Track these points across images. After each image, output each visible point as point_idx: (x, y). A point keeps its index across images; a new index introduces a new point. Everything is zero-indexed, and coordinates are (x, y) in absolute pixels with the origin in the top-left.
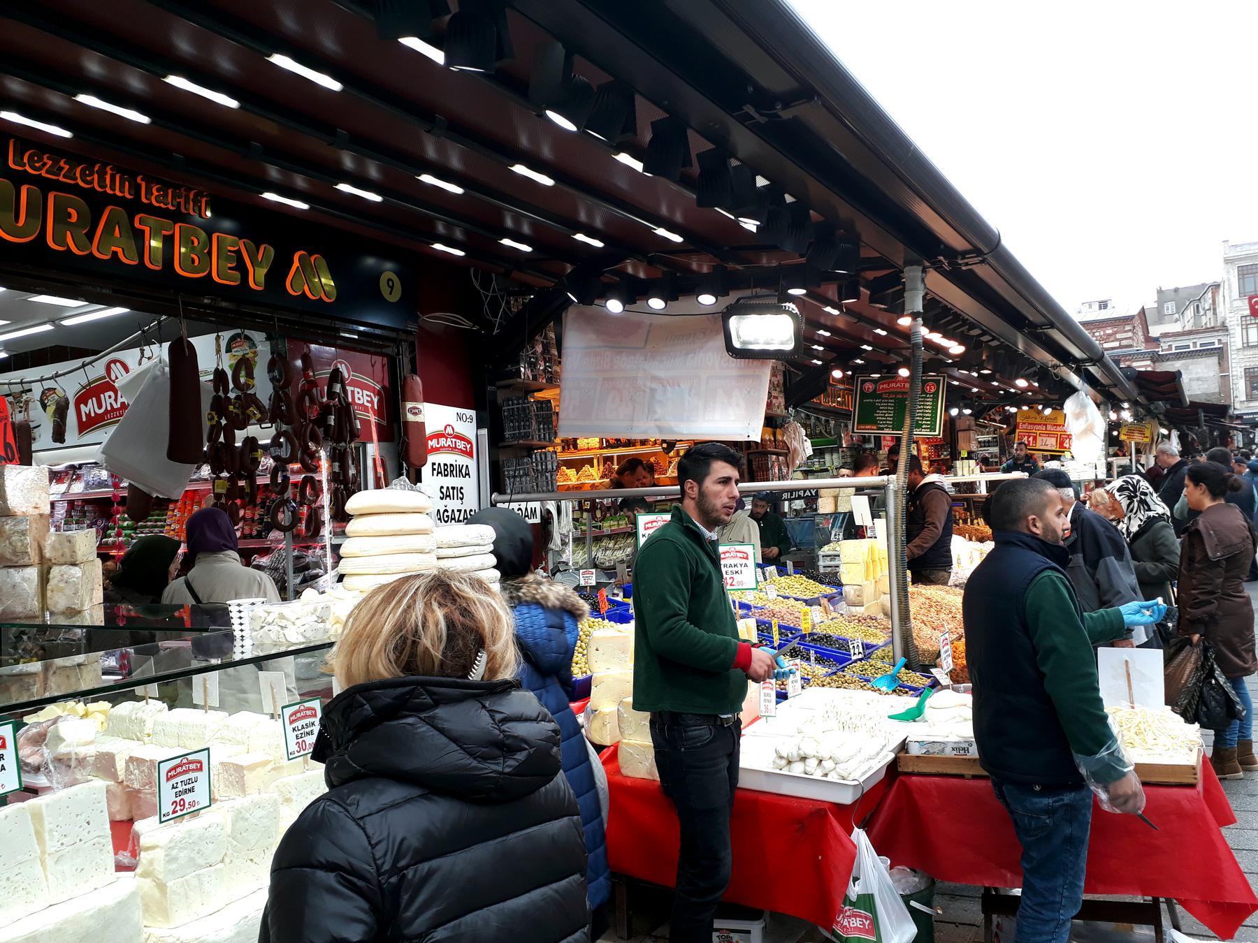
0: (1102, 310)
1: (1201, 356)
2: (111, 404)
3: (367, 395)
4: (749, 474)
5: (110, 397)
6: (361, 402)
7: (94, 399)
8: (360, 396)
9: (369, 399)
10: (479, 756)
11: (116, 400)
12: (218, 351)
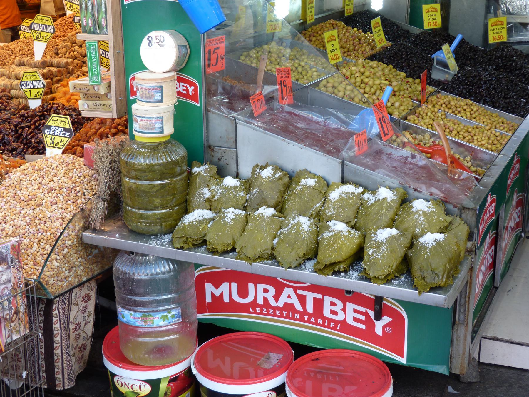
2: (265, 299)
3: (183, 86)
9: (185, 88)
11: (277, 297)
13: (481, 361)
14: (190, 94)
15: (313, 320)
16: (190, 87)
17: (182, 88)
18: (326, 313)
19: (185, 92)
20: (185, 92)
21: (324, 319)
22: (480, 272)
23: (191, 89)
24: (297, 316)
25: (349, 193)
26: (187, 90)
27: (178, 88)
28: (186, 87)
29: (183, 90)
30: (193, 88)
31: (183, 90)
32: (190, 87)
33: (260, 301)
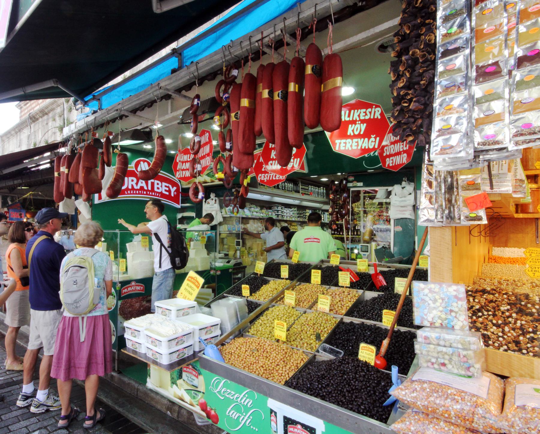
0: (321, 241)
1: (324, 112)
2: (132, 185)
3: (166, 186)
4: (183, 212)
5: (132, 181)
6: (159, 191)
7: (299, 159)
8: (159, 186)
9: (167, 189)
10: (527, 314)
11: (137, 184)
12: (261, 314)
13: (282, 266)
14: (172, 195)
15: (151, 193)
16: (173, 187)
17: (164, 188)
18: (156, 190)
19: (167, 193)
20: (167, 193)
21: (155, 192)
22: (455, 336)
23: (173, 190)
24: (145, 193)
25: (466, 393)
26: (169, 191)
27: (160, 188)
28: (168, 187)
29: (166, 191)
30: (175, 188)
31: (166, 191)
32: (173, 187)
33: (130, 187)
